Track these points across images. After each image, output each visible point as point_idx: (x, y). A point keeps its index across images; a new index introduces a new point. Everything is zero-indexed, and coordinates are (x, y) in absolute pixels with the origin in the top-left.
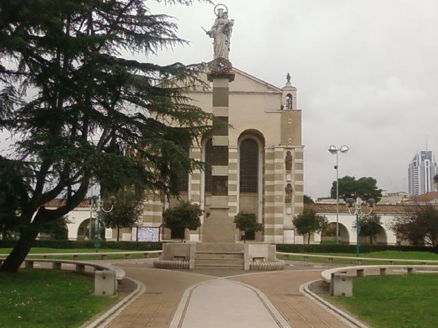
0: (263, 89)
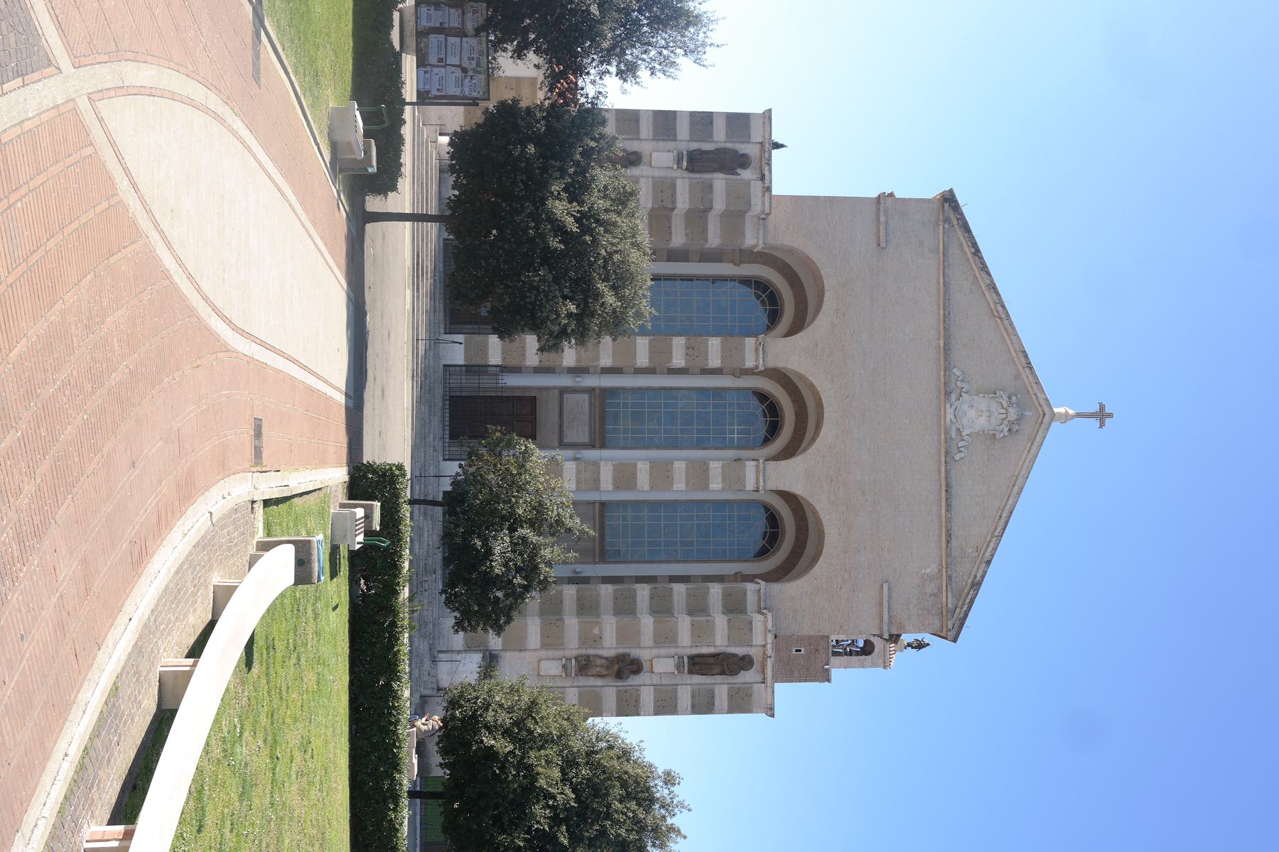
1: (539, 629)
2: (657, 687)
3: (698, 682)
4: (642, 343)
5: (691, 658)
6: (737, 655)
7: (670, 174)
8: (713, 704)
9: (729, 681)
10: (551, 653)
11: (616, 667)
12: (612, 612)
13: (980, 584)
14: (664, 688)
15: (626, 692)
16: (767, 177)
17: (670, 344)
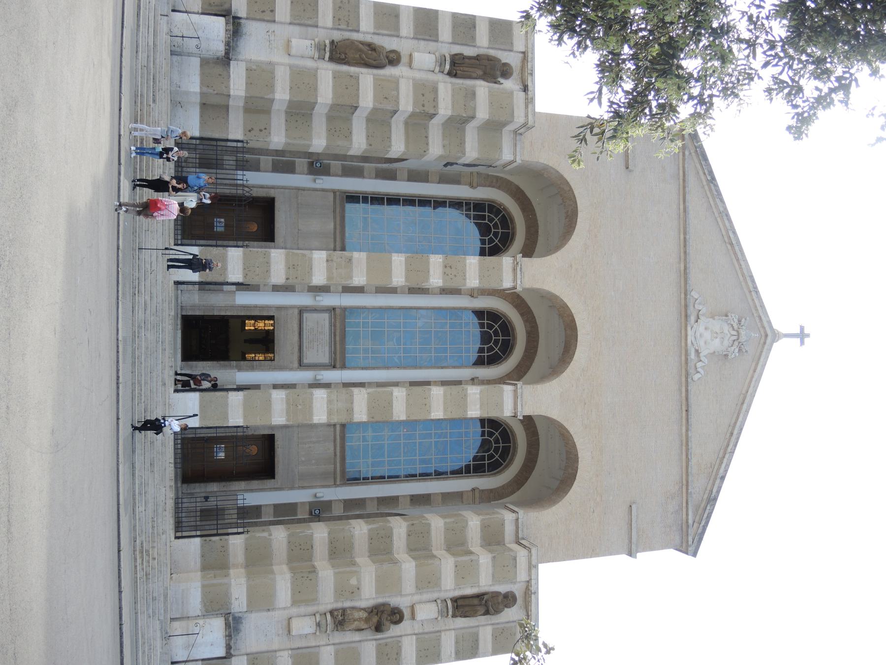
0: (698, 485)
1: (289, 585)
2: (420, 636)
3: (462, 626)
4: (398, 261)
5: (455, 600)
6: (500, 593)
7: (432, 77)
8: (477, 648)
9: (493, 622)
10: (303, 610)
11: (375, 619)
12: (367, 554)
13: (715, 499)
14: (426, 636)
15: (386, 645)
16: (530, 88)
17: (428, 263)
